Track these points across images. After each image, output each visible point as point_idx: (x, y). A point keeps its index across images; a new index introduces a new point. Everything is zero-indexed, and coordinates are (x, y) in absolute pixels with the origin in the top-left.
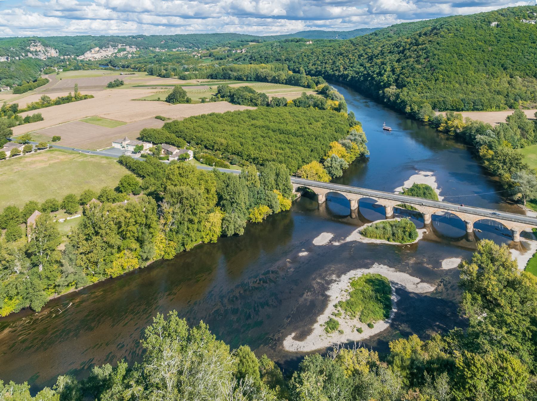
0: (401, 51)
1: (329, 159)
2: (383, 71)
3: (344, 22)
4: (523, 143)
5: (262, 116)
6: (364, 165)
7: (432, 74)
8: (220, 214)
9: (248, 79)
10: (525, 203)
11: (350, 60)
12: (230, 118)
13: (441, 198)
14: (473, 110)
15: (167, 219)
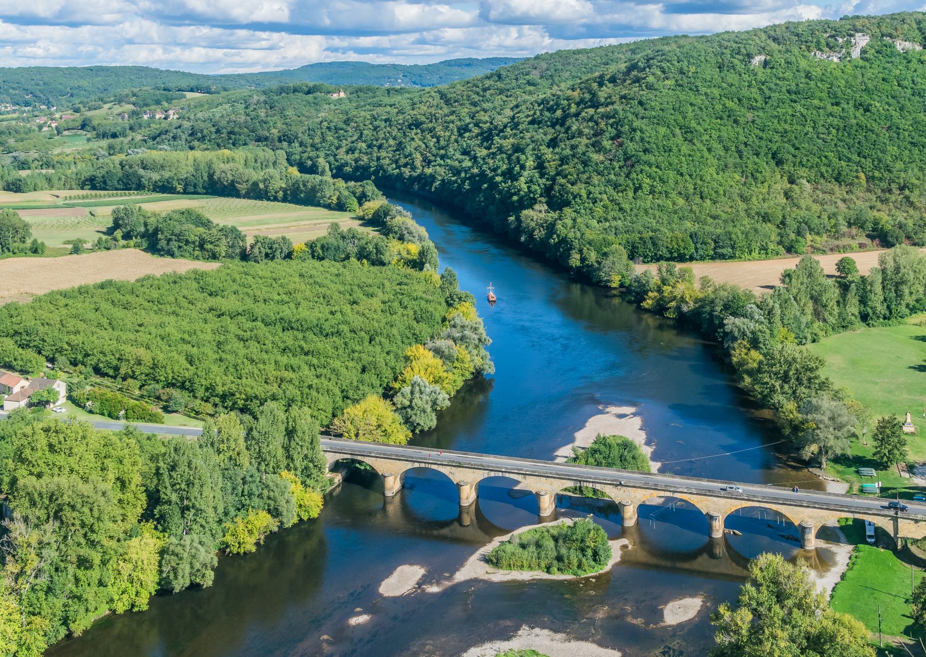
0: (556, 117)
1: (407, 389)
2: (517, 168)
3: (422, 42)
4: (817, 331)
5: (235, 287)
6: (481, 398)
7: (628, 176)
8: (154, 540)
9: (190, 189)
10: (824, 466)
11: (438, 138)
12: (155, 294)
13: (655, 466)
14: (713, 258)
15: (25, 562)
